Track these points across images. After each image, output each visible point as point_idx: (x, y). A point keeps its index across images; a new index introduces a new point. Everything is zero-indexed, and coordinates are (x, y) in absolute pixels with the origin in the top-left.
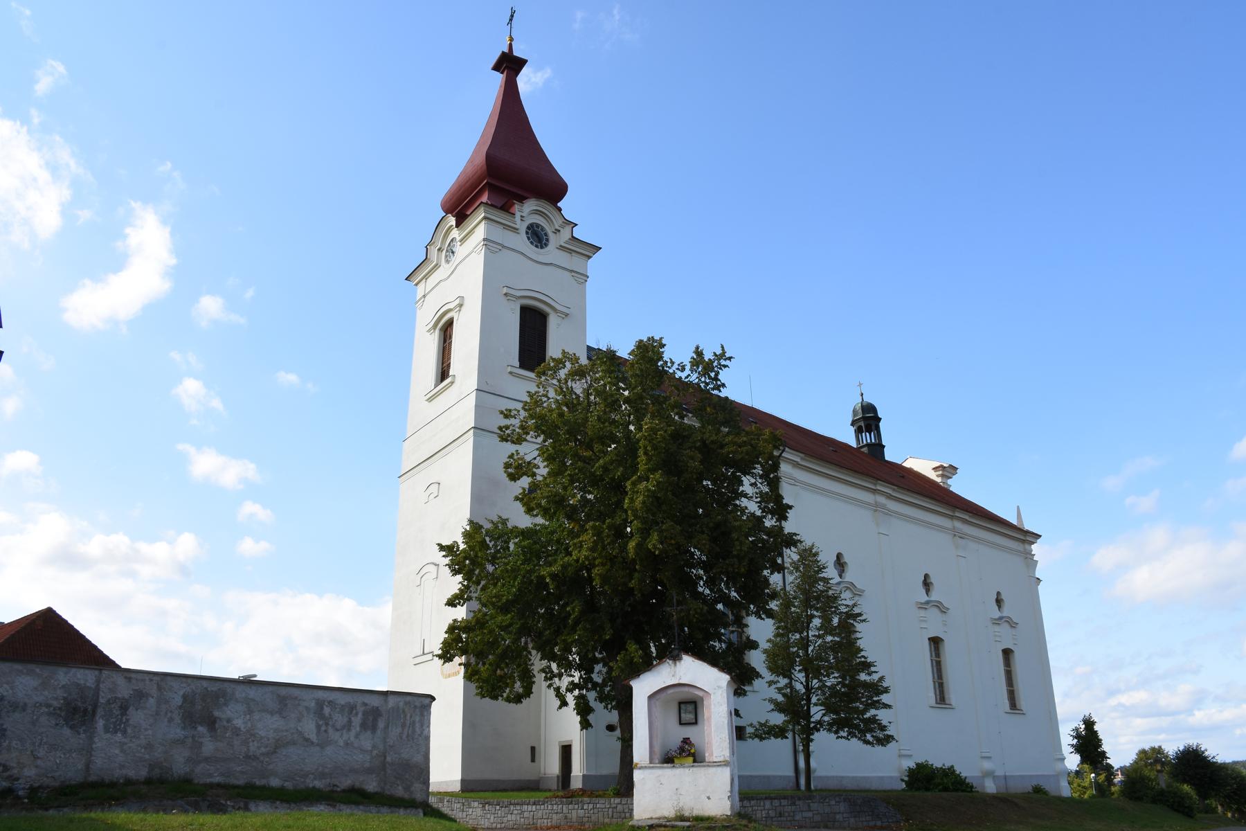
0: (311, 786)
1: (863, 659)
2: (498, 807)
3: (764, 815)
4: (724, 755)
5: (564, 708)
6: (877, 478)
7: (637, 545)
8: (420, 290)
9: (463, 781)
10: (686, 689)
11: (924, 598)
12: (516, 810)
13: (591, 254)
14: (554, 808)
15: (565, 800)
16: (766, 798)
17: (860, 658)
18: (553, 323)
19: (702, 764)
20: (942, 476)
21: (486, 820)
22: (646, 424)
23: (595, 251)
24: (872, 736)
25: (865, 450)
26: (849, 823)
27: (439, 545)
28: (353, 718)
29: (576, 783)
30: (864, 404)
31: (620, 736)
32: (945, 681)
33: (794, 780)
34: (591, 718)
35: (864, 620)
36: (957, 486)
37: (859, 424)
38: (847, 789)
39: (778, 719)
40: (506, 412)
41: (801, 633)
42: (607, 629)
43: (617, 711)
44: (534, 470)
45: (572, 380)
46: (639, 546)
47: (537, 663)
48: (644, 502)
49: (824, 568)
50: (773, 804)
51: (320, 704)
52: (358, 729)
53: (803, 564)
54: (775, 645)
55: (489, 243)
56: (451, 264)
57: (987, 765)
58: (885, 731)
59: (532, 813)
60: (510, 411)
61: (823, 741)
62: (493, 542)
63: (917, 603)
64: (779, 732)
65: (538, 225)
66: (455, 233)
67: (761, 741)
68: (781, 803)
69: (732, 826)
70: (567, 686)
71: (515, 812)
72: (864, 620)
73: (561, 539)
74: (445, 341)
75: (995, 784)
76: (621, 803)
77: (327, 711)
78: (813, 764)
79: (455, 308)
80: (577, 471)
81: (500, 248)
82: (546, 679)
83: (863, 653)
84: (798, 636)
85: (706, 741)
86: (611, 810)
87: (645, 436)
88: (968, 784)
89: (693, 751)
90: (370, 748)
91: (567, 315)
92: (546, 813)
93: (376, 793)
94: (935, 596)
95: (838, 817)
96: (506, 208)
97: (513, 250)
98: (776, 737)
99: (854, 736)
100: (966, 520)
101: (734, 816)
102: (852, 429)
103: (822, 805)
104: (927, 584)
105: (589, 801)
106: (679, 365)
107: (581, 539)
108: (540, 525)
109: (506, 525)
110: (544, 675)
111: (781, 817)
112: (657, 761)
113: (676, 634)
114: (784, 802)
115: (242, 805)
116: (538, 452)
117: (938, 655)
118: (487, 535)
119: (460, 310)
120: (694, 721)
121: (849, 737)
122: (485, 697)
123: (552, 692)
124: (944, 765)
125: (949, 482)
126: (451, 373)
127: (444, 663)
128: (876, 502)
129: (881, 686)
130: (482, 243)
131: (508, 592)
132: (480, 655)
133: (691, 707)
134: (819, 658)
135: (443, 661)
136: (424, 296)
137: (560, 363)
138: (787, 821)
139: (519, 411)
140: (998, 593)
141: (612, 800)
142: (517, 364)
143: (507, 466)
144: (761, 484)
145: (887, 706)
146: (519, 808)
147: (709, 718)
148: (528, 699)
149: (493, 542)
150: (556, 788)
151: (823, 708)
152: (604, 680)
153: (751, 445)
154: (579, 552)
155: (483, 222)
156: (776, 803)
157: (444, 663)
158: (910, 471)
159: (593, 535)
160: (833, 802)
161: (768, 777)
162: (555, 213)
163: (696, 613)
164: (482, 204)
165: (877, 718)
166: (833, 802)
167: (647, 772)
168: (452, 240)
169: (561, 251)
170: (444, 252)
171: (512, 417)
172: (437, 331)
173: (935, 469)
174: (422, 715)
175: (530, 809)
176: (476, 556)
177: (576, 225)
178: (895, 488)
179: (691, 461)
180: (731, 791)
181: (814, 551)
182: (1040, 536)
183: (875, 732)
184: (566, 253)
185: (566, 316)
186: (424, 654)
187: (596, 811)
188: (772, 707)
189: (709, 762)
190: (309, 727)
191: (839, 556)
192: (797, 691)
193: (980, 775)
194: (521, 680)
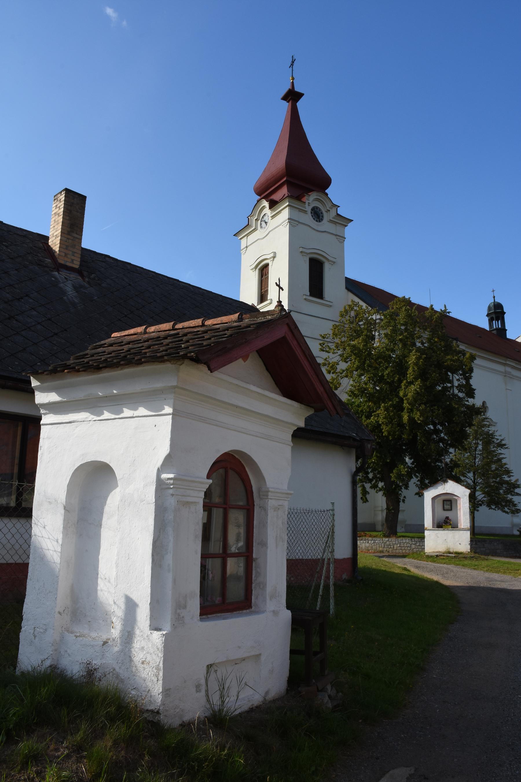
18: (327, 267)
19: (456, 529)
25: (495, 332)
30: (495, 304)
37: (492, 316)
58: (516, 507)
65: (317, 208)
72: (507, 448)
79: (270, 258)
81: (297, 223)
83: (506, 466)
86: (383, 544)
91: (334, 262)
102: (487, 319)
112: (436, 527)
119: (273, 260)
120: (450, 509)
126: (269, 297)
130: (288, 221)
133: (449, 503)
136: (247, 247)
141: (384, 539)
142: (308, 293)
159: (385, 411)
160: (496, 544)
167: (431, 532)
168: (265, 215)
170: (259, 221)
172: (257, 270)
177: (339, 207)
178: (517, 362)
185: (334, 263)
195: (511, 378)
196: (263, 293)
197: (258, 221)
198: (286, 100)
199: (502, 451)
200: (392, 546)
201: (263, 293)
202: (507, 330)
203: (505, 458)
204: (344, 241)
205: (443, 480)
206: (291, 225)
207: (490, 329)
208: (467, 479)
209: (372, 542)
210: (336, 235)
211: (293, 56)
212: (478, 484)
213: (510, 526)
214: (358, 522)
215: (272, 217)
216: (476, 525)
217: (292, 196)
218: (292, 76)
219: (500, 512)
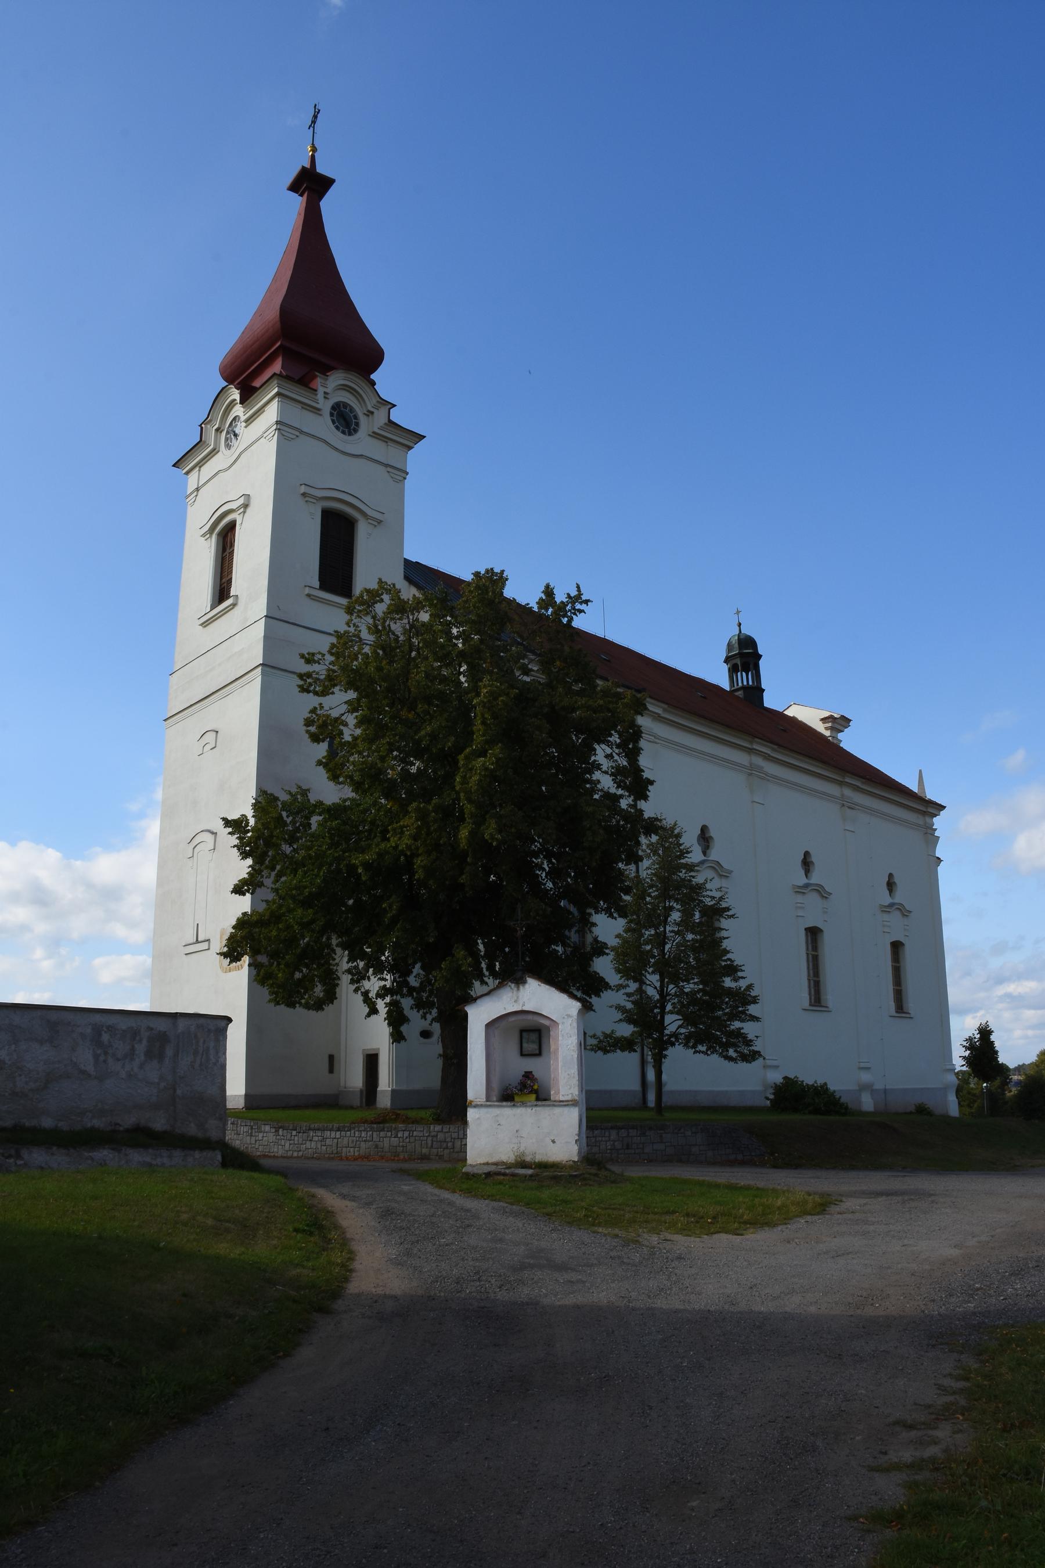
0: (89, 1125)
1: (729, 962)
2: (294, 1133)
5: (374, 1017)
6: (753, 734)
7: (470, 833)
8: (192, 481)
9: (247, 1096)
10: (530, 1017)
11: (803, 881)
12: (316, 1136)
13: (410, 444)
14: (363, 1135)
15: (375, 1126)
16: (612, 1128)
17: (725, 961)
18: (362, 530)
19: (544, 1103)
20: (832, 729)
22: (485, 686)
23: (418, 440)
24: (735, 1051)
25: (740, 694)
27: (224, 819)
28: (136, 1046)
29: (384, 1101)
30: (742, 637)
31: (441, 1052)
32: (821, 979)
33: (641, 1095)
34: (404, 1029)
35: (732, 916)
36: (850, 742)
37: (734, 662)
39: (626, 1030)
40: (307, 656)
41: (656, 928)
43: (439, 1024)
44: (341, 727)
45: (392, 619)
46: (472, 833)
47: (343, 962)
49: (688, 852)
50: (620, 1133)
51: (98, 1030)
52: (143, 1058)
53: (662, 846)
54: (625, 941)
55: (282, 427)
56: (233, 449)
57: (866, 1077)
59: (335, 1140)
60: (313, 654)
61: (678, 1056)
62: (291, 818)
63: (794, 886)
64: (626, 1044)
65: (345, 405)
66: (238, 410)
67: (605, 1054)
68: (628, 1133)
69: (581, 1175)
70: (378, 991)
71: (316, 1139)
72: (732, 916)
74: (224, 550)
75: (872, 1099)
76: (442, 1131)
77: (105, 1037)
78: (664, 1077)
79: (239, 508)
80: (397, 738)
81: (297, 433)
82: (352, 982)
83: (729, 956)
85: (552, 1076)
86: (430, 1139)
87: (483, 702)
88: (843, 1104)
89: (536, 1087)
90: (156, 1080)
91: (380, 522)
92: (353, 1141)
93: (165, 1132)
94: (815, 878)
96: (304, 382)
98: (622, 1050)
99: (714, 1051)
100: (858, 787)
101: (582, 1162)
102: (725, 668)
104: (807, 863)
105: (404, 1129)
107: (402, 823)
108: (348, 799)
109: (307, 796)
110: (350, 977)
111: (628, 1149)
113: (520, 953)
114: (633, 1132)
115: (13, 1152)
116: (346, 706)
117: (815, 948)
118: (283, 809)
119: (244, 512)
120: (537, 1052)
121: (709, 1052)
122: (280, 1004)
123: (359, 998)
124: (816, 1082)
125: (840, 736)
127: (230, 962)
130: (275, 427)
131: (311, 883)
132: (274, 955)
133: (534, 1036)
134: (678, 959)
135: (229, 960)
136: (197, 489)
137: (374, 596)
138: (635, 1153)
139: (324, 655)
140: (891, 876)
142: (317, 584)
143: (308, 723)
144: (618, 755)
145: (754, 1019)
146: (320, 1134)
148: (330, 1005)
149: (291, 818)
150: (359, 1105)
151: (681, 1018)
152: (421, 983)
153: (609, 710)
154: (400, 838)
156: (623, 1133)
157: (230, 962)
158: (793, 721)
159: (417, 820)
160: (689, 1133)
161: (610, 1092)
162: (366, 387)
164: (275, 377)
165: (742, 1031)
166: (689, 1133)
167: (483, 1110)
168: (235, 419)
169: (374, 439)
170: (224, 434)
171: (315, 662)
172: (214, 537)
173: (824, 720)
174: (217, 1040)
175: (333, 1135)
176: (271, 836)
177: (394, 406)
178: (776, 747)
179: (537, 733)
180: (579, 1135)
181: (676, 832)
182: (945, 807)
183: (740, 1047)
184: (380, 442)
185: (379, 523)
186: (197, 942)
187: (412, 1139)
188: (619, 1016)
189: (555, 1101)
190: (85, 1057)
191: (704, 829)
192: (649, 997)
193: (857, 1088)
194: (323, 982)
195: (763, 779)
196: (223, 586)
197: (221, 432)
198: (297, 193)
200: (450, 1144)
201: (223, 586)
202: (764, 690)
203: (727, 938)
204: (405, 478)
206: (284, 435)
209: (406, 1134)
210: (388, 465)
211: (316, 105)
214: (227, 1094)
215: (246, 421)
216: (666, 1089)
217: (288, 376)
218: (313, 144)
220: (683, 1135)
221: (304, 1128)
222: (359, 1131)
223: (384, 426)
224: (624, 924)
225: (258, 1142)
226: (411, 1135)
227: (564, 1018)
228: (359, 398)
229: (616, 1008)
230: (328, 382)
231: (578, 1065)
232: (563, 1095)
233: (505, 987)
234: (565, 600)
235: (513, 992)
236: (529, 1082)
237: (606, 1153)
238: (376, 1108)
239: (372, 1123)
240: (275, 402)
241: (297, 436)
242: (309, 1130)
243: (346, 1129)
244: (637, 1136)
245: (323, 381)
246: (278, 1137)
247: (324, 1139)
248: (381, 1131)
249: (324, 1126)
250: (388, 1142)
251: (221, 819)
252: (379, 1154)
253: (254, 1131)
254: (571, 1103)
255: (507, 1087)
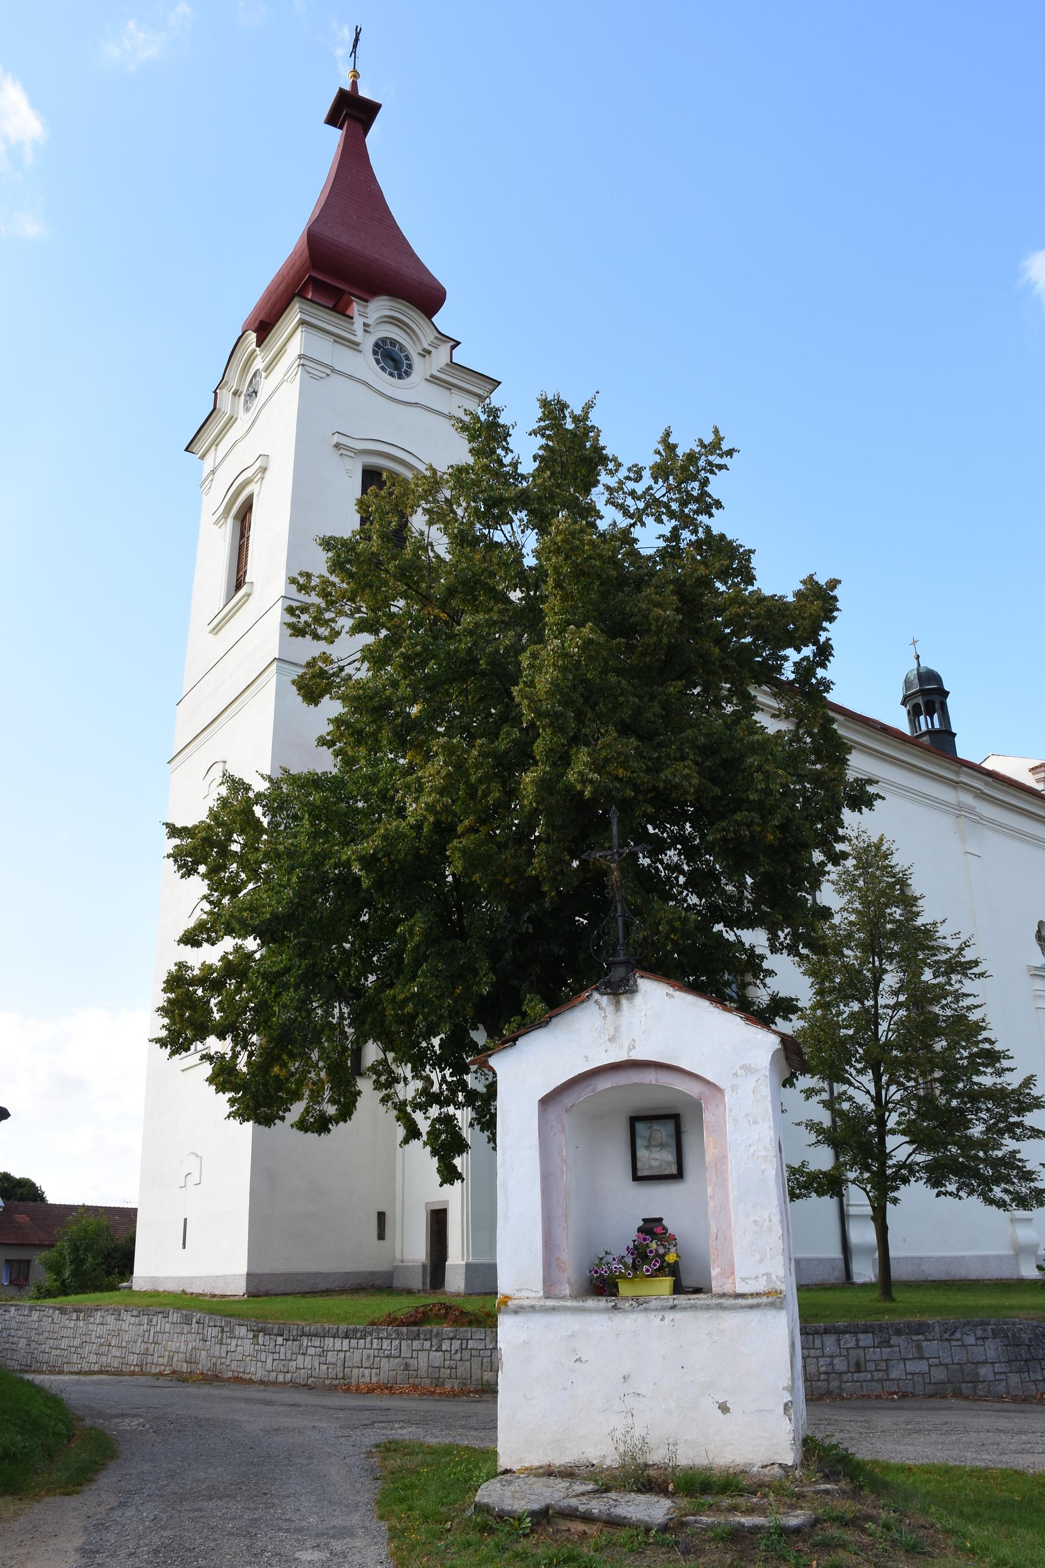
1: (987, 1046)
2: (280, 1340)
3: (823, 1369)
4: (768, 1275)
10: (649, 1077)
15: (404, 1329)
16: (826, 1331)
17: (982, 1041)
21: (259, 1364)
25: (926, 739)
26: (1007, 1387)
27: (167, 825)
30: (921, 671)
33: (841, 1265)
35: (982, 975)
37: (915, 701)
38: (930, 1278)
42: (481, 975)
48: (554, 683)
56: (252, 410)
58: (1033, 1180)
59: (342, 1355)
65: (393, 342)
68: (857, 1340)
72: (982, 975)
73: (388, 790)
79: (255, 474)
81: (329, 371)
83: (985, 1034)
84: (856, 1006)
85: (713, 1229)
89: (671, 1258)
92: (369, 1357)
95: (983, 1371)
96: (340, 308)
97: (350, 377)
98: (820, 1194)
102: (903, 711)
103: (946, 1344)
105: (452, 1335)
106: (629, 470)
111: (859, 1371)
114: (866, 1340)
120: (674, 1170)
128: (959, 802)
129: (1029, 1094)
130: (297, 363)
133: (664, 1132)
135: (168, 1050)
136: (213, 472)
138: (872, 1380)
146: (317, 1344)
147: (722, 1159)
151: (907, 1139)
155: (300, 329)
156: (849, 1340)
160: (971, 1340)
163: (673, 930)
166: (971, 1340)
167: (538, 1320)
168: (255, 375)
170: (243, 397)
172: (230, 521)
175: (338, 1347)
177: (458, 343)
187: (466, 1355)
188: (812, 1137)
189: (723, 1295)
197: (240, 396)
199: (968, 986)
205: (608, 985)
207: (912, 733)
208: (851, 1091)
209: (456, 1344)
212: (891, 1106)
213: (1010, 1252)
216: (892, 1253)
219: (975, 1202)
220: (959, 1343)
221: (295, 1332)
222: (378, 1338)
223: (445, 368)
224: (811, 995)
225: (229, 1354)
226: (464, 1346)
227: (736, 1074)
228: (413, 337)
229: (807, 1126)
230: (368, 311)
231: (779, 1197)
232: (743, 1279)
233: (585, 1004)
234: (697, 449)
235: (605, 1018)
236: (653, 1245)
237: (819, 1380)
238: (444, 1293)
239: (402, 1324)
240: (298, 335)
241: (328, 375)
242: (301, 1336)
243: (358, 1335)
244: (874, 1347)
245: (362, 309)
246: (257, 1347)
247: (323, 1351)
248: (414, 1339)
249: (324, 1329)
250: (426, 1359)
251: (163, 824)
252: (411, 1380)
253: (225, 1334)
254: (764, 1300)
255: (601, 1259)
